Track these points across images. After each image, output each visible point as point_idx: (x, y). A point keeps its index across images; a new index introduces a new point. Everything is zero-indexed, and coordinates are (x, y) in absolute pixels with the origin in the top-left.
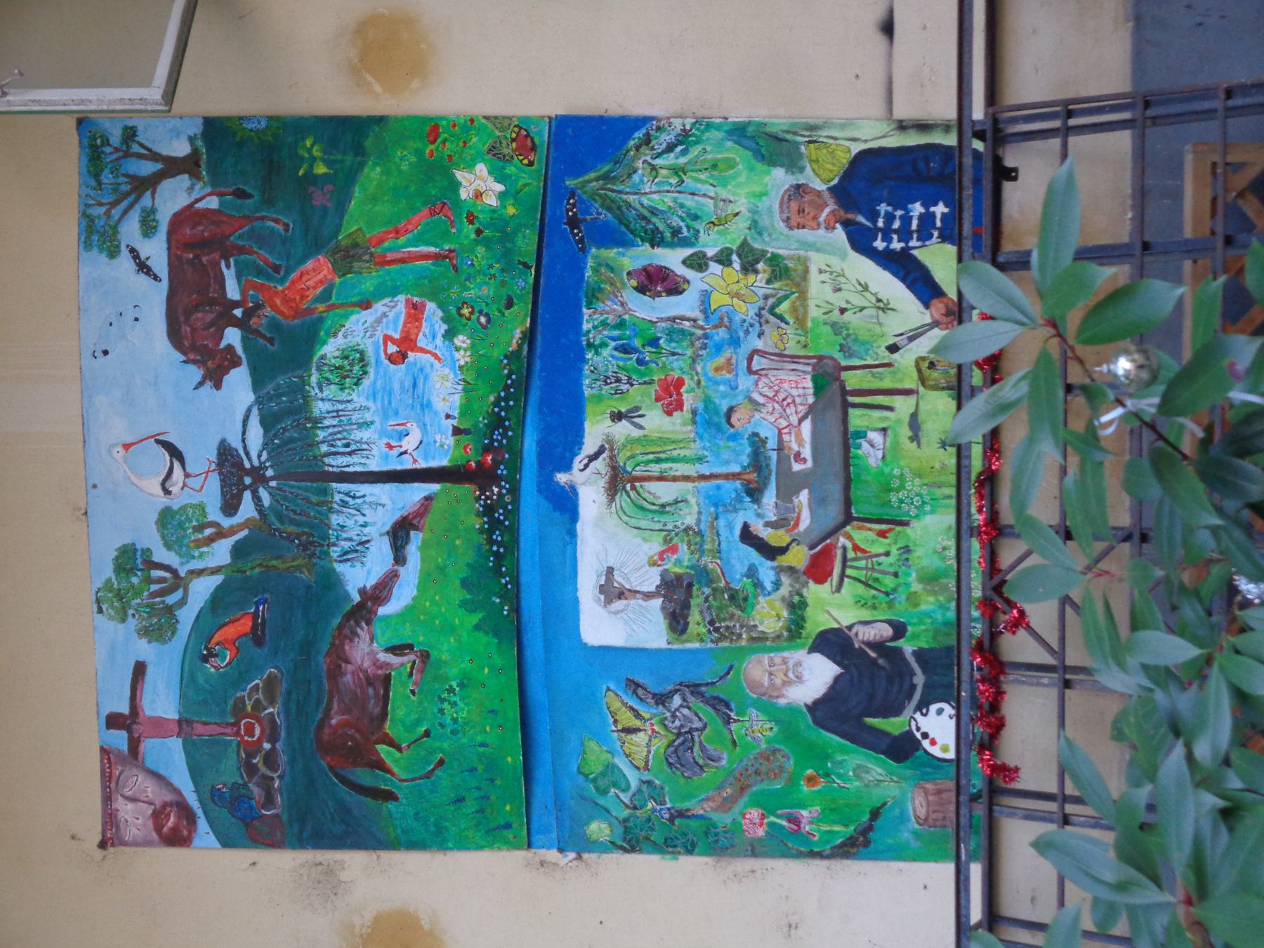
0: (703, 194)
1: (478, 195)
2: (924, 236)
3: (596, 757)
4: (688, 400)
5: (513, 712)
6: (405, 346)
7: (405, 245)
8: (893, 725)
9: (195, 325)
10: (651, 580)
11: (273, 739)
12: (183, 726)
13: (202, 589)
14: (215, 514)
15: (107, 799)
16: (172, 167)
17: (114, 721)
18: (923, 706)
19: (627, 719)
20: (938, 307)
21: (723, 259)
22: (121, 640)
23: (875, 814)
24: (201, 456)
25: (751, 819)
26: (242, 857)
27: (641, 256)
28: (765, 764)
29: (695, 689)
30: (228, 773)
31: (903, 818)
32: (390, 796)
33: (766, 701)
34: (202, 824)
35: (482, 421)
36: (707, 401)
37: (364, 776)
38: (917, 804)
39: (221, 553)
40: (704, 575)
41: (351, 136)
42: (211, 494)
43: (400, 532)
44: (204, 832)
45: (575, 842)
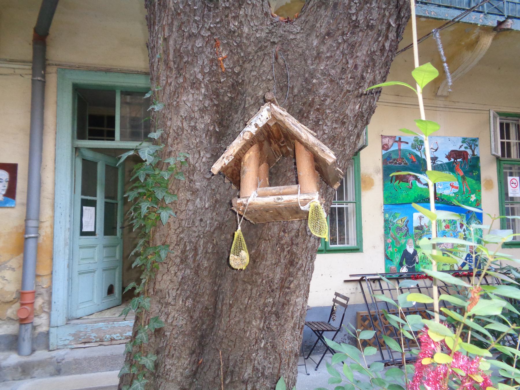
2: (469, 265)
3: (398, 215)
4: (447, 229)
5: (404, 202)
6: (453, 186)
7: (465, 186)
8: (404, 263)
9: (455, 154)
10: (423, 224)
11: (399, 164)
12: (400, 149)
13: (418, 153)
15: (388, 137)
16: (473, 152)
17: (400, 139)
18: (407, 267)
19: (403, 220)
20: (460, 267)
21: (465, 235)
22: (411, 142)
23: (391, 260)
25: (390, 240)
26: (380, 157)
28: (398, 242)
29: (408, 231)
30: (394, 156)
31: (391, 265)
32: (391, 182)
33: (407, 242)
34: (386, 152)
35: (443, 198)
36: (447, 232)
38: (393, 267)
40: (423, 232)
41: (478, 178)
44: (384, 152)
45: (385, 212)
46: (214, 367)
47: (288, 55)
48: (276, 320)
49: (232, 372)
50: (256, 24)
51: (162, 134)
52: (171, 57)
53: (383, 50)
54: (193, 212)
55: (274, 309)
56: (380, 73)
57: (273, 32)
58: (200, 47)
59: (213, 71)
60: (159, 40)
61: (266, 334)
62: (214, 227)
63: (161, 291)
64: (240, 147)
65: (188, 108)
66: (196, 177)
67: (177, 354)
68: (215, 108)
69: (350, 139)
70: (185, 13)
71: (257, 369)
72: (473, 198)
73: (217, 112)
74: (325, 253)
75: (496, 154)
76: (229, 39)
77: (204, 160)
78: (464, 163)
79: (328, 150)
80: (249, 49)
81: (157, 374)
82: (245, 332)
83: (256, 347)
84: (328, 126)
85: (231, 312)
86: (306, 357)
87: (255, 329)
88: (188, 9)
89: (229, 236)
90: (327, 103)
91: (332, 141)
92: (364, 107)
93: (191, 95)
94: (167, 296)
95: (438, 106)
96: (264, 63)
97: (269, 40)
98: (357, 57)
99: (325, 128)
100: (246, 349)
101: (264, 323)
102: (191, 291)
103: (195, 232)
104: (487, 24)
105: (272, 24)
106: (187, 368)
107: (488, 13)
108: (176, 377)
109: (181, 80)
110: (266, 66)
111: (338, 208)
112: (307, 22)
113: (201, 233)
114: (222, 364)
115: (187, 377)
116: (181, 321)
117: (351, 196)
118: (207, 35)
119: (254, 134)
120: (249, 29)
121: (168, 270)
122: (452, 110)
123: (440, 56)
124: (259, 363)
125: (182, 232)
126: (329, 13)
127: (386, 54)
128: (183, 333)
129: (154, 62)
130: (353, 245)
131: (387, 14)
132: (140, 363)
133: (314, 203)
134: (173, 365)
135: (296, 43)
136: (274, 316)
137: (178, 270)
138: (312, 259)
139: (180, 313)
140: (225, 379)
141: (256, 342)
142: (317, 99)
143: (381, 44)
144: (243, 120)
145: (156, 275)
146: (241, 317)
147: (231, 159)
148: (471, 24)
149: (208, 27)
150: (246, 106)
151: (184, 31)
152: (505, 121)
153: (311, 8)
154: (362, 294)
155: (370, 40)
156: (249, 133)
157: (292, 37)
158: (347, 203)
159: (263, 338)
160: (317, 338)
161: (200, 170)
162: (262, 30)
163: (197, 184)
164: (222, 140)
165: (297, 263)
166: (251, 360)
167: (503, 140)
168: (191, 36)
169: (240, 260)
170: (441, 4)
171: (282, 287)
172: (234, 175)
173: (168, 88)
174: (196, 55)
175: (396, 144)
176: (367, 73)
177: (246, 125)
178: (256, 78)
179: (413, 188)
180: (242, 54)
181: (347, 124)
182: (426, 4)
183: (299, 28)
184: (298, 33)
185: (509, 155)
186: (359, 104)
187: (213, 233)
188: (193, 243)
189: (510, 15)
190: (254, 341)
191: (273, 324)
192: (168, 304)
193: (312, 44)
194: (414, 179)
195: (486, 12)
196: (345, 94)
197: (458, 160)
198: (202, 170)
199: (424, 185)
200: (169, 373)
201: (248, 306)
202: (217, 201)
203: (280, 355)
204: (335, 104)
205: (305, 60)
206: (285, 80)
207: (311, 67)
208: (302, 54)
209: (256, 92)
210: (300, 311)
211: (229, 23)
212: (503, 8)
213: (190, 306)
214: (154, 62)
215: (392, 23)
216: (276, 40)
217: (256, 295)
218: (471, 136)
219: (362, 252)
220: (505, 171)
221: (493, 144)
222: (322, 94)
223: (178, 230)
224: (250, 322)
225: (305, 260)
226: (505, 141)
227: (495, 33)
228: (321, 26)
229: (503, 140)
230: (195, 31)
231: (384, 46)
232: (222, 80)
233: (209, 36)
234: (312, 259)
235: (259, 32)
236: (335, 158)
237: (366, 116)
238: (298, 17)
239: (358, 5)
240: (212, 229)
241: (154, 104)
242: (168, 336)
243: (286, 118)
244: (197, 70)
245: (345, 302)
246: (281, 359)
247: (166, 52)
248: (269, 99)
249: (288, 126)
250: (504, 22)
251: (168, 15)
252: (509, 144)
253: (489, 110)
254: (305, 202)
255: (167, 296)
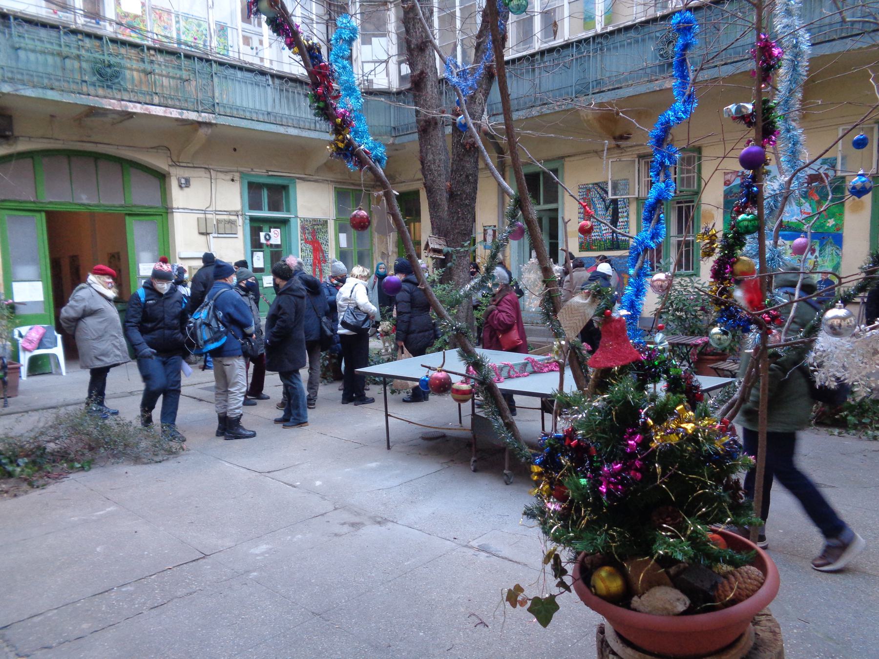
0: (828, 258)
1: (587, 116)
26: (722, 194)
27: (817, 248)
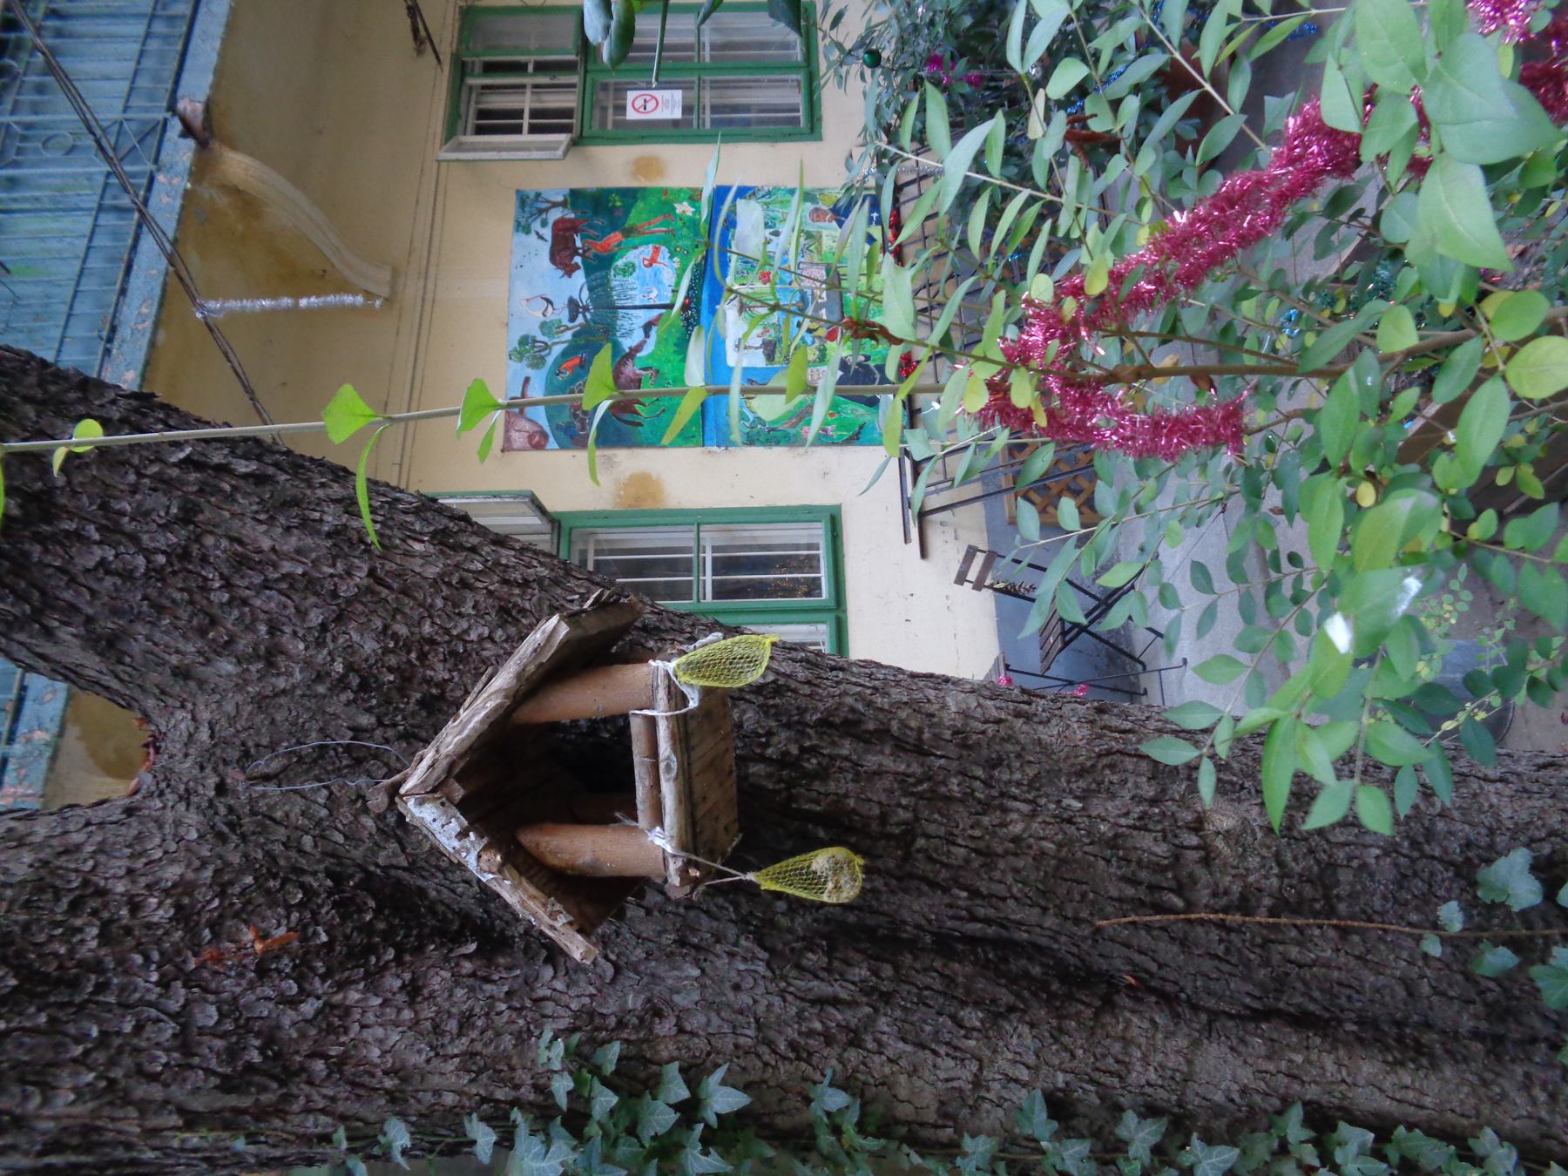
6: (652, 261)
9: (562, 254)
10: (759, 342)
13: (557, 350)
14: (565, 322)
15: (507, 431)
16: (555, 205)
23: (861, 427)
24: (561, 302)
26: (566, 455)
32: (640, 424)
34: (551, 439)
37: (628, 417)
39: (568, 336)
41: (630, 195)
42: (564, 316)
43: (647, 328)
44: (552, 443)
45: (725, 442)
46: (1144, 939)
47: (257, 745)
48: (1009, 766)
49: (1152, 888)
50: (157, 841)
51: (482, 1119)
52: (246, 1102)
53: (259, 479)
54: (713, 1015)
55: (979, 772)
56: (323, 485)
57: (187, 790)
58: (219, 1010)
59: (295, 967)
60: (188, 1146)
61: (1047, 795)
62: (757, 949)
63: (942, 1103)
64: (524, 880)
65: (405, 1041)
66: (610, 1007)
67: (1117, 1048)
68: (408, 958)
69: (507, 566)
70: (112, 1063)
71: (1140, 818)
72: (684, 208)
73: (419, 950)
74: (845, 611)
75: (563, 147)
76: (197, 923)
77: (559, 985)
78: (589, 229)
79: (536, 637)
80: (236, 859)
81: (1176, 1110)
82: (1043, 853)
83: (1082, 821)
84: (470, 627)
85: (992, 896)
86: (1140, 667)
87: (1035, 825)
88: (100, 1057)
89: (781, 905)
90: (403, 630)
91: (514, 620)
92: (418, 527)
93: (366, 1034)
94: (955, 1084)
95: (420, 293)
96: (279, 814)
97: (211, 801)
98: (273, 549)
99: (473, 636)
100: (1087, 848)
101: (1015, 798)
102: (940, 1014)
103: (770, 1006)
104: (188, 164)
105: (161, 794)
106: (1152, 1021)
107: (156, 161)
108: (1178, 1052)
109: (319, 1065)
110: (287, 808)
111: (715, 573)
112: (163, 692)
113: (772, 987)
114: (1133, 918)
115: (1176, 1016)
116: (1021, 1039)
117: (682, 538)
118: (183, 991)
119: (485, 840)
120: (173, 861)
121: (883, 1084)
122: (433, 259)
123: (273, 312)
124: (1126, 814)
125: (770, 1044)
126: (141, 629)
127: (271, 470)
128: (1058, 1033)
129: (256, 1156)
130: (821, 532)
131: (154, 469)
132: (1147, 1161)
133: (680, 673)
134: (1145, 1060)
135: (223, 722)
136: (996, 773)
137: (881, 1053)
138: (842, 669)
139: (1001, 1043)
140: (1172, 910)
141: (1070, 821)
142: (392, 660)
143: (242, 483)
144: (444, 871)
145: (897, 1122)
146: (1002, 864)
147: (558, 907)
148: (183, 207)
149: (158, 990)
150: (405, 864)
151: (166, 1065)
152: (472, 121)
153: (121, 680)
154: (957, 510)
155: (227, 514)
156: (485, 857)
157: (204, 735)
158: (700, 548)
159: (1059, 802)
160: (1084, 635)
161: (591, 996)
162: (178, 823)
163: (630, 1006)
164: (502, 932)
165: (853, 710)
166: (1116, 836)
167: (525, 128)
168: (185, 1043)
169: (832, 875)
170: (118, 286)
171: (919, 750)
172: (599, 897)
173: (341, 1107)
174: (242, 1022)
175: (529, 411)
176: (321, 520)
177: (460, 864)
178: (323, 837)
179: (655, 365)
180: (249, 880)
181: (465, 574)
182: (113, 329)
183: (180, 714)
184: (194, 719)
185: (568, 113)
186: (410, 542)
187: (772, 951)
188: (803, 1010)
189: (165, 104)
190: (1065, 826)
191: (1017, 776)
192: (977, 1083)
193: (229, 676)
194: (630, 363)
195: (153, 167)
196: (380, 581)
197: (579, 243)
198: (592, 990)
199: (647, 335)
200: (1169, 1073)
201: (972, 845)
202: (682, 942)
203: (1100, 756)
204: (407, 610)
205: (276, 695)
206: (332, 753)
207: (298, 676)
208: (260, 702)
209: (365, 835)
210: (982, 701)
211: (150, 926)
212: (144, 122)
213: (980, 1015)
214: (256, 1156)
215: (182, 455)
216: (212, 781)
217: (941, 824)
218: (511, 206)
219: (839, 507)
220: (610, 126)
221: (536, 155)
222: (376, 646)
223: (766, 1057)
224: (1016, 840)
225: (842, 687)
226: (526, 121)
227: (215, 145)
228: (178, 652)
229: (525, 128)
230: (170, 1029)
231: (245, 476)
232: (324, 938)
233: (185, 985)
234: (842, 669)
235: (182, 831)
236: (555, 619)
237: (445, 521)
238: (146, 718)
239: (122, 549)
240: (765, 955)
241: (390, 1147)
242: (1070, 1077)
243: (443, 751)
244: (288, 1017)
245: (979, 559)
246: (1109, 753)
247: (229, 1122)
248: (386, 800)
249: (466, 745)
250: (184, 121)
251: (113, 1119)
252: (535, 114)
253: (439, 161)
254: (677, 697)
255: (955, 1084)
